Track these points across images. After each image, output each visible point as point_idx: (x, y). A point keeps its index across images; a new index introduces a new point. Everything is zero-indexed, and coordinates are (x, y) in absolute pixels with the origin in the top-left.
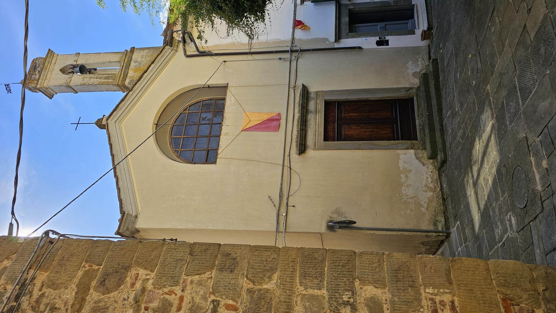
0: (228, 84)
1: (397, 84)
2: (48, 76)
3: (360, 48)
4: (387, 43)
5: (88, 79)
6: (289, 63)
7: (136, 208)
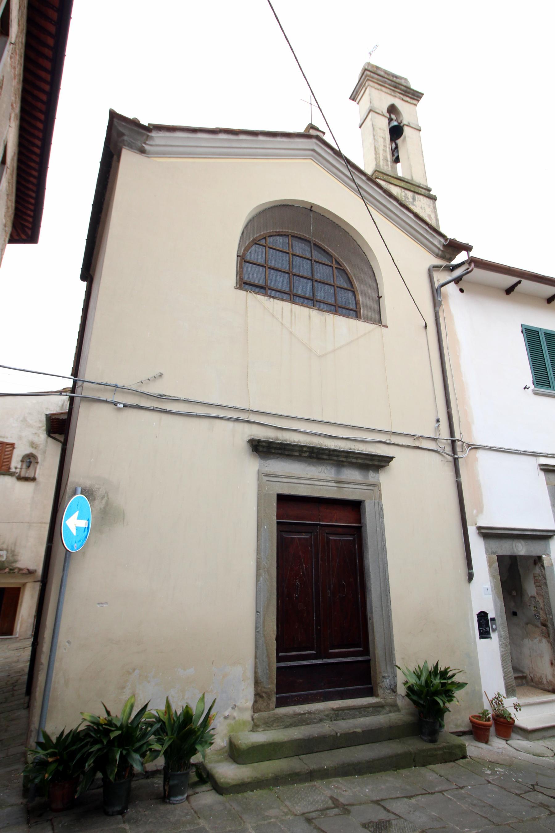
0: (386, 327)
1: (403, 659)
2: (384, 89)
3: (470, 577)
4: (484, 634)
5: (382, 135)
6: (432, 436)
7: (160, 154)
